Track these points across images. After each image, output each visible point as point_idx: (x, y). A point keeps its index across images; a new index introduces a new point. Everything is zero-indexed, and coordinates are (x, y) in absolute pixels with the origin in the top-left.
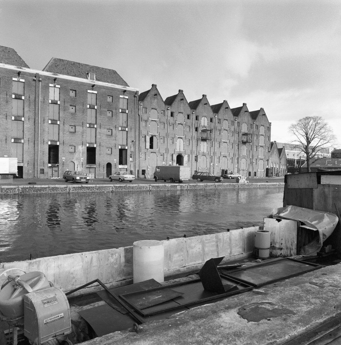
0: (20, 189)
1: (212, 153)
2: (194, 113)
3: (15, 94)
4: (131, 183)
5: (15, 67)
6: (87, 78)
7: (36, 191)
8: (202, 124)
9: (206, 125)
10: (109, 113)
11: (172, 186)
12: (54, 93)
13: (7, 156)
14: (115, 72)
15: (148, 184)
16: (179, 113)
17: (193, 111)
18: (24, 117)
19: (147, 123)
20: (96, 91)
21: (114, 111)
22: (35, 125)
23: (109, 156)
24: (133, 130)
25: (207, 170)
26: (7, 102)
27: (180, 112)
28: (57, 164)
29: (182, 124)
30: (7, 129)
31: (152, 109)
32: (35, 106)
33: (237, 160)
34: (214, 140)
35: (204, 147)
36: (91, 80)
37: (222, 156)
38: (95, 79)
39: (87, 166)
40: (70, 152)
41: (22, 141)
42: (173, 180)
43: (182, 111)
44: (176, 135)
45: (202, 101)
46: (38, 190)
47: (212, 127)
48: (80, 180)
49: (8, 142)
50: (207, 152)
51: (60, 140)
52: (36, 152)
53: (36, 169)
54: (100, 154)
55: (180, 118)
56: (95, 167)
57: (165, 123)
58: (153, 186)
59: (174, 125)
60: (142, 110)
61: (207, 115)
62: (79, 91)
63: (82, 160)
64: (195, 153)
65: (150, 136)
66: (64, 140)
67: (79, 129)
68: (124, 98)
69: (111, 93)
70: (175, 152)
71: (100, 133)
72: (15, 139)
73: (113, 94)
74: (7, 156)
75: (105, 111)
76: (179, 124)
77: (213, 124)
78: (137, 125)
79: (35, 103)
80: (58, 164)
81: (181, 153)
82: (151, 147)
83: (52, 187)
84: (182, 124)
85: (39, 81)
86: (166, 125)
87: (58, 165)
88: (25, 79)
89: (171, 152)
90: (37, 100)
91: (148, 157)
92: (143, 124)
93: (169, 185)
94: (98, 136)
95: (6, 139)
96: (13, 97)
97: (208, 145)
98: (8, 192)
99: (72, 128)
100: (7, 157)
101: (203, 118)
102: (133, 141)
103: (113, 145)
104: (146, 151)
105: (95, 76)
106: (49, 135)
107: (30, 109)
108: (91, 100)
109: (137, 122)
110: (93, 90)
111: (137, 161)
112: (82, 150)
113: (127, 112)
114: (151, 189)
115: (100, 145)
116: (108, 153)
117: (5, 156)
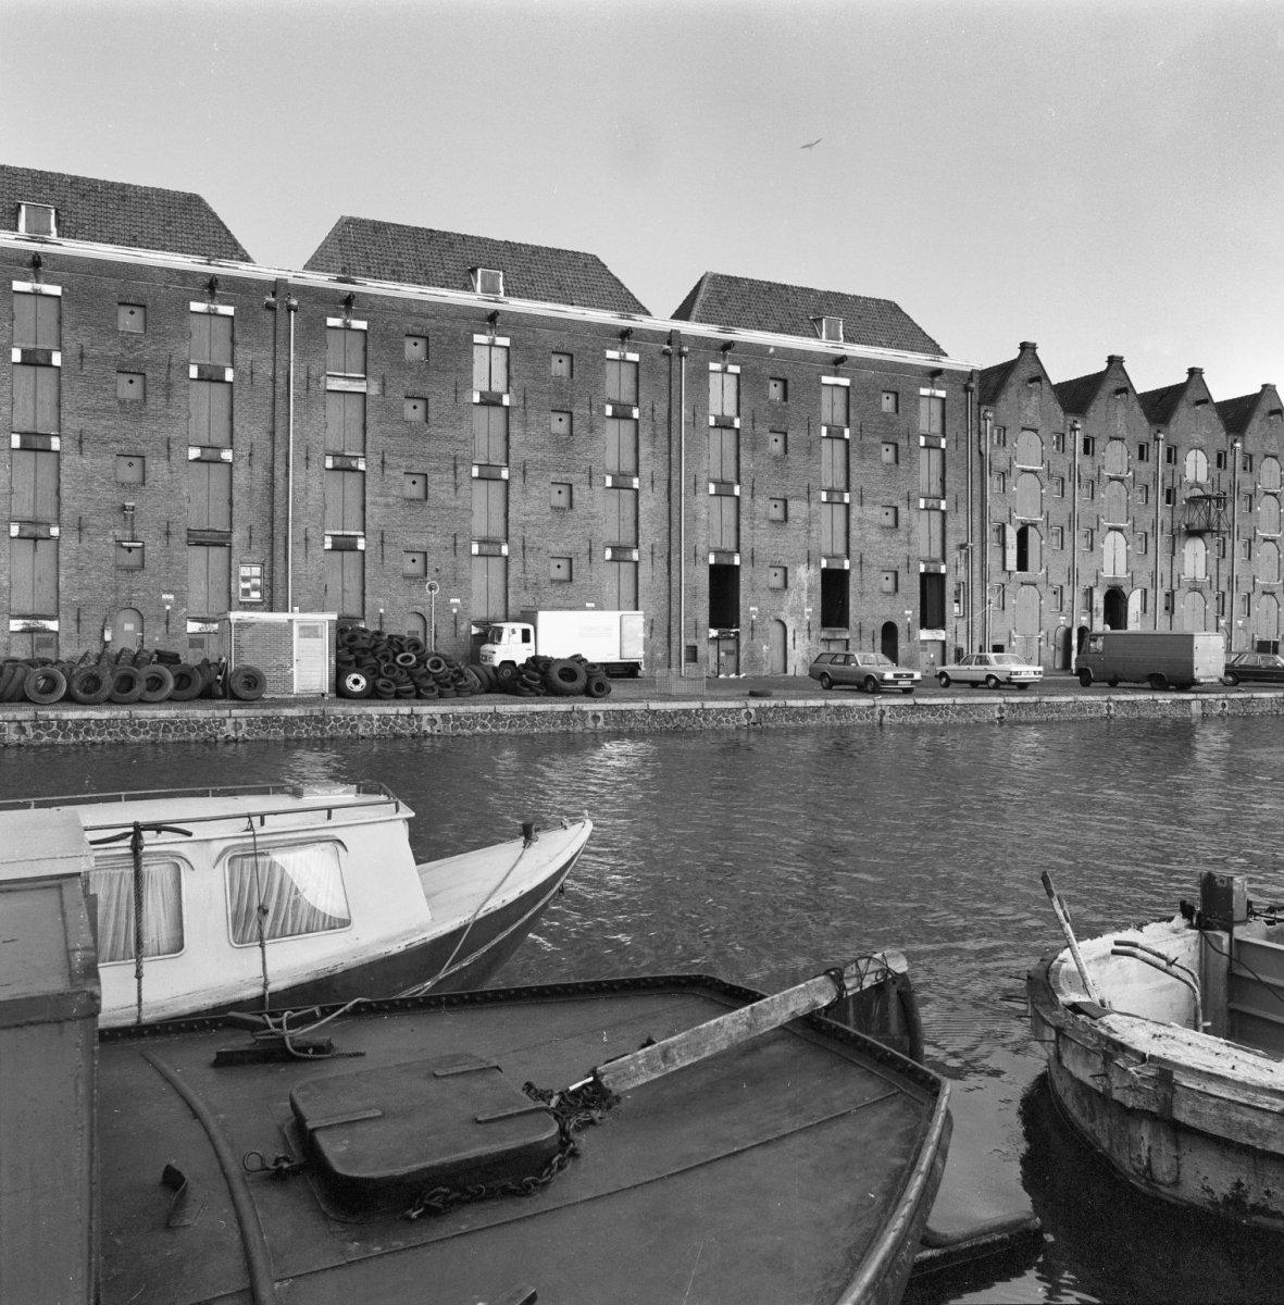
0: (752, 712)
1: (1223, 579)
2: (1162, 436)
3: (615, 404)
4: (1022, 692)
5: (614, 314)
6: (817, 336)
7: (793, 719)
8: (1190, 477)
9: (1202, 478)
10: (415, 407)
11: (1175, 703)
12: (722, 395)
13: (593, 605)
14: (894, 308)
15: (1103, 694)
16: (1111, 439)
17: (1159, 431)
18: (638, 476)
19: (1007, 481)
20: (362, 320)
21: (902, 443)
22: (669, 500)
23: (888, 598)
24: (962, 506)
25: (1042, 643)
26: (591, 431)
27: (1113, 435)
28: (734, 630)
29: (1121, 480)
30: (593, 517)
31: (1023, 429)
32: (670, 437)
33: (1215, 603)
34: (1231, 533)
35: (1195, 557)
36: (832, 343)
37: (1258, 592)
38: (842, 336)
39: (824, 635)
40: (771, 589)
41: (635, 555)
42: (1159, 683)
43: (1122, 432)
44: (1102, 520)
45: (1189, 393)
46: (798, 713)
47: (1225, 486)
48: (896, 683)
49: (595, 559)
50: (1208, 578)
51: (742, 548)
52: (673, 591)
53: (674, 646)
54: (862, 594)
55: (1116, 458)
56: (847, 637)
57: (1067, 478)
58: (1118, 702)
59: (1096, 483)
60: (992, 434)
61: (1204, 442)
62: (445, 340)
63: (808, 613)
64: (1167, 583)
65: (1019, 526)
66: (756, 549)
67: (795, 507)
68: (37, 294)
69: (893, 380)
70: (1100, 581)
71: (860, 521)
72: (614, 549)
73: (581, 348)
74: (593, 605)
75: (877, 446)
76: (1111, 479)
77: (1226, 476)
78: (977, 490)
79: (670, 429)
80: (738, 627)
81: (1118, 582)
82: (1022, 564)
83: (835, 707)
84: (1121, 480)
85: (681, 354)
86: (1068, 485)
87: (737, 633)
88: (640, 353)
89: (1086, 581)
90: (675, 417)
91: (1010, 601)
92: (993, 483)
93: (1164, 698)
94: (855, 533)
95: (590, 550)
96: (13, 360)
97: (1208, 552)
98: (720, 721)
99: (414, 483)
100: (592, 609)
101: (1191, 455)
102: (962, 546)
103: (902, 561)
104: (1003, 578)
105: (841, 327)
106: (710, 529)
107: (656, 450)
108: (831, 409)
109: (977, 477)
110: (836, 374)
111: (978, 615)
112: (806, 577)
113: (943, 446)
114: (1112, 712)
115: (861, 562)
116: (885, 590)
117: (588, 605)
